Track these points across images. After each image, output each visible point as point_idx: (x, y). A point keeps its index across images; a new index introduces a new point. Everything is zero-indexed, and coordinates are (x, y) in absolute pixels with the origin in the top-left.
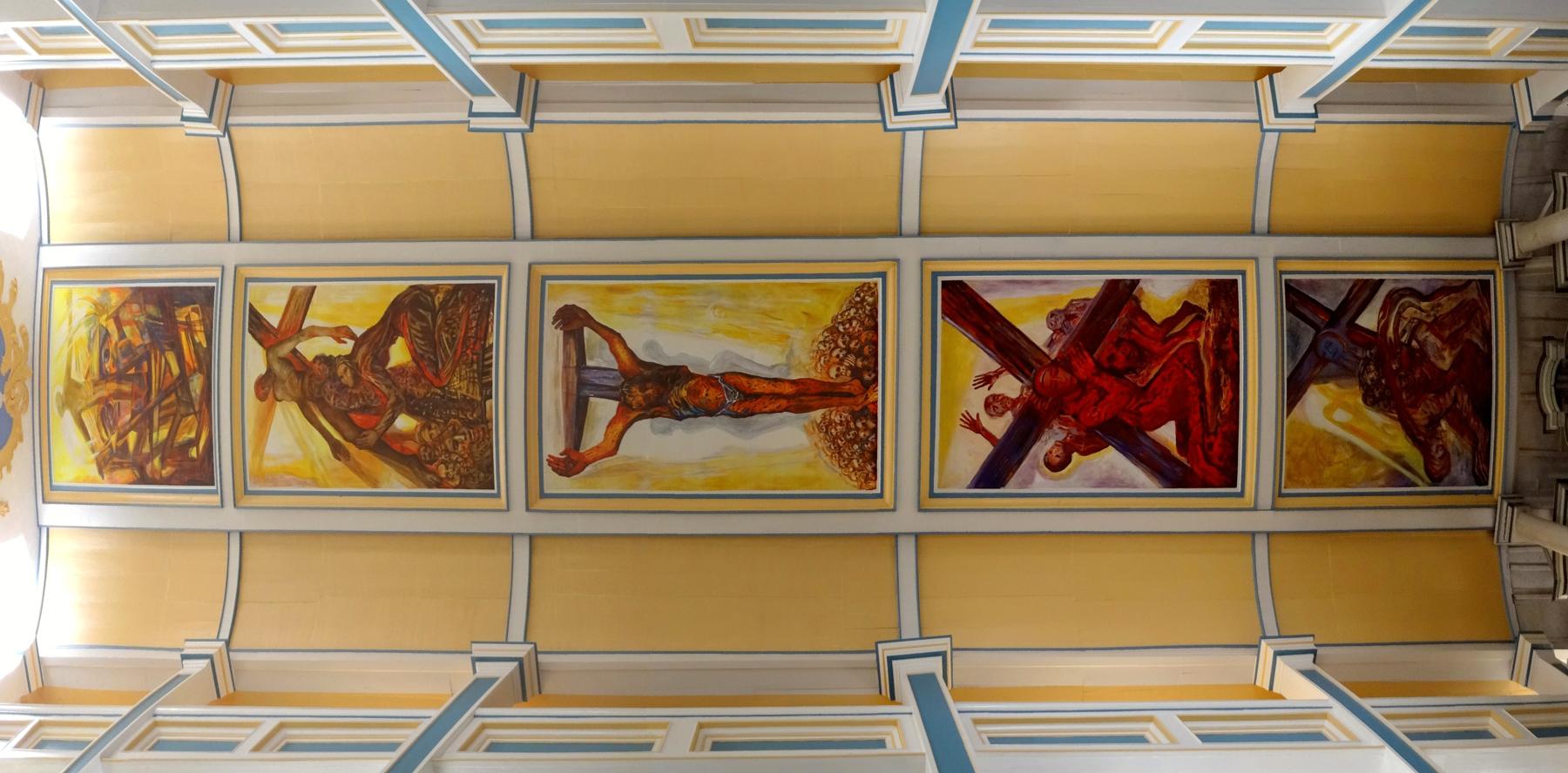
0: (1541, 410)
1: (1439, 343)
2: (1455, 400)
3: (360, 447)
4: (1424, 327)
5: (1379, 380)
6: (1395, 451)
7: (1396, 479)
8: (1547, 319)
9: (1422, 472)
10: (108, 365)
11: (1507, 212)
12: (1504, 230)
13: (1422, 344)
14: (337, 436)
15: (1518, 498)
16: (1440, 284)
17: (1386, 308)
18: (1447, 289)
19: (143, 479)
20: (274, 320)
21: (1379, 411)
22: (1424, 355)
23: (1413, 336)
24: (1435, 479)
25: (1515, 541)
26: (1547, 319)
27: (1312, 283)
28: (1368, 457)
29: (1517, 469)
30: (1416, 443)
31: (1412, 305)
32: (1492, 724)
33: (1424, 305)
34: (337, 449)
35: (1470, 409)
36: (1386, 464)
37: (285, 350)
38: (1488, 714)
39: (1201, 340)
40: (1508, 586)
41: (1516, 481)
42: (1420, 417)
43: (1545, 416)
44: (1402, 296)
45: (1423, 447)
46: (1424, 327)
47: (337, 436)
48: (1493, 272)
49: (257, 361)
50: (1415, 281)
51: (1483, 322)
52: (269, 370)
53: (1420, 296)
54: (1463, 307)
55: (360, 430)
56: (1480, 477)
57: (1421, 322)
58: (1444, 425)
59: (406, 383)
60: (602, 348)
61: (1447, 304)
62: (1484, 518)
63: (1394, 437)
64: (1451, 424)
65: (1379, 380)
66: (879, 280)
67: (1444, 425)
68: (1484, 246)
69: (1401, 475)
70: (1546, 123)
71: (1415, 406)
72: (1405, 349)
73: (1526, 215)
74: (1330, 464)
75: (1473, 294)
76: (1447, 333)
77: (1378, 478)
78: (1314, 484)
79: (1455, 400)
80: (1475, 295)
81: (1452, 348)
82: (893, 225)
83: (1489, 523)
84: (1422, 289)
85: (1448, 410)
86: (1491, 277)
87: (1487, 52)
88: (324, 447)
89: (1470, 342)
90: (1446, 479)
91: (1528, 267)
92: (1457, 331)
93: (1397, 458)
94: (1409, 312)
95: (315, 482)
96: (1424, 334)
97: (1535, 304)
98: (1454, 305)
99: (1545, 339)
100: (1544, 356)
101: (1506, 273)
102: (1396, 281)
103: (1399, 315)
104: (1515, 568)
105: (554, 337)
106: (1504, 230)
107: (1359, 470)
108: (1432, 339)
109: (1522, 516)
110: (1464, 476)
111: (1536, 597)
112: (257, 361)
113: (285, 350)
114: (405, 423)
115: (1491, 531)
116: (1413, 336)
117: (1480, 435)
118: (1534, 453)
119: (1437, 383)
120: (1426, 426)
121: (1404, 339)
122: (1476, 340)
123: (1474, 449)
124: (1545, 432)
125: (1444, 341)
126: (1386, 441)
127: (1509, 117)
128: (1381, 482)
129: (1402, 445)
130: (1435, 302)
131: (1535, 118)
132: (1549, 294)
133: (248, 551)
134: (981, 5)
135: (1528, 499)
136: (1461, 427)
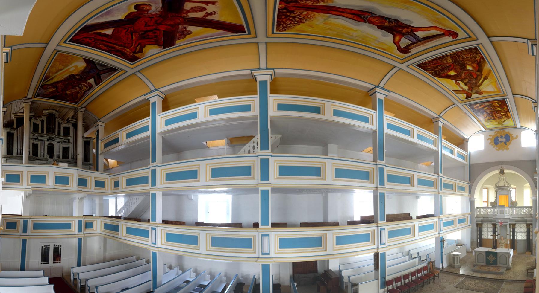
3: (482, 75)
7: (47, 78)
13: (76, 89)
14: (482, 79)
19: (508, 111)
20: (465, 95)
22: (73, 88)
23: (79, 87)
27: (112, 74)
28: (56, 72)
30: (54, 83)
34: (485, 78)
37: (470, 91)
39: (128, 50)
47: (482, 79)
49: (475, 96)
52: (476, 93)
55: (478, 76)
56: (39, 95)
57: (81, 89)
58: (54, 89)
59: (459, 70)
60: (402, 43)
62: (30, 96)
66: (275, 32)
67: (54, 89)
74: (60, 64)
77: (49, 73)
78: (56, 60)
82: (258, 67)
88: (486, 81)
93: (52, 79)
95: (496, 82)
105: (413, 51)
107: (54, 70)
110: (40, 92)
112: (475, 96)
113: (470, 91)
114: (469, 68)
115: (26, 97)
116: (79, 87)
129: (55, 80)
133: (517, 93)
134: (280, 1)
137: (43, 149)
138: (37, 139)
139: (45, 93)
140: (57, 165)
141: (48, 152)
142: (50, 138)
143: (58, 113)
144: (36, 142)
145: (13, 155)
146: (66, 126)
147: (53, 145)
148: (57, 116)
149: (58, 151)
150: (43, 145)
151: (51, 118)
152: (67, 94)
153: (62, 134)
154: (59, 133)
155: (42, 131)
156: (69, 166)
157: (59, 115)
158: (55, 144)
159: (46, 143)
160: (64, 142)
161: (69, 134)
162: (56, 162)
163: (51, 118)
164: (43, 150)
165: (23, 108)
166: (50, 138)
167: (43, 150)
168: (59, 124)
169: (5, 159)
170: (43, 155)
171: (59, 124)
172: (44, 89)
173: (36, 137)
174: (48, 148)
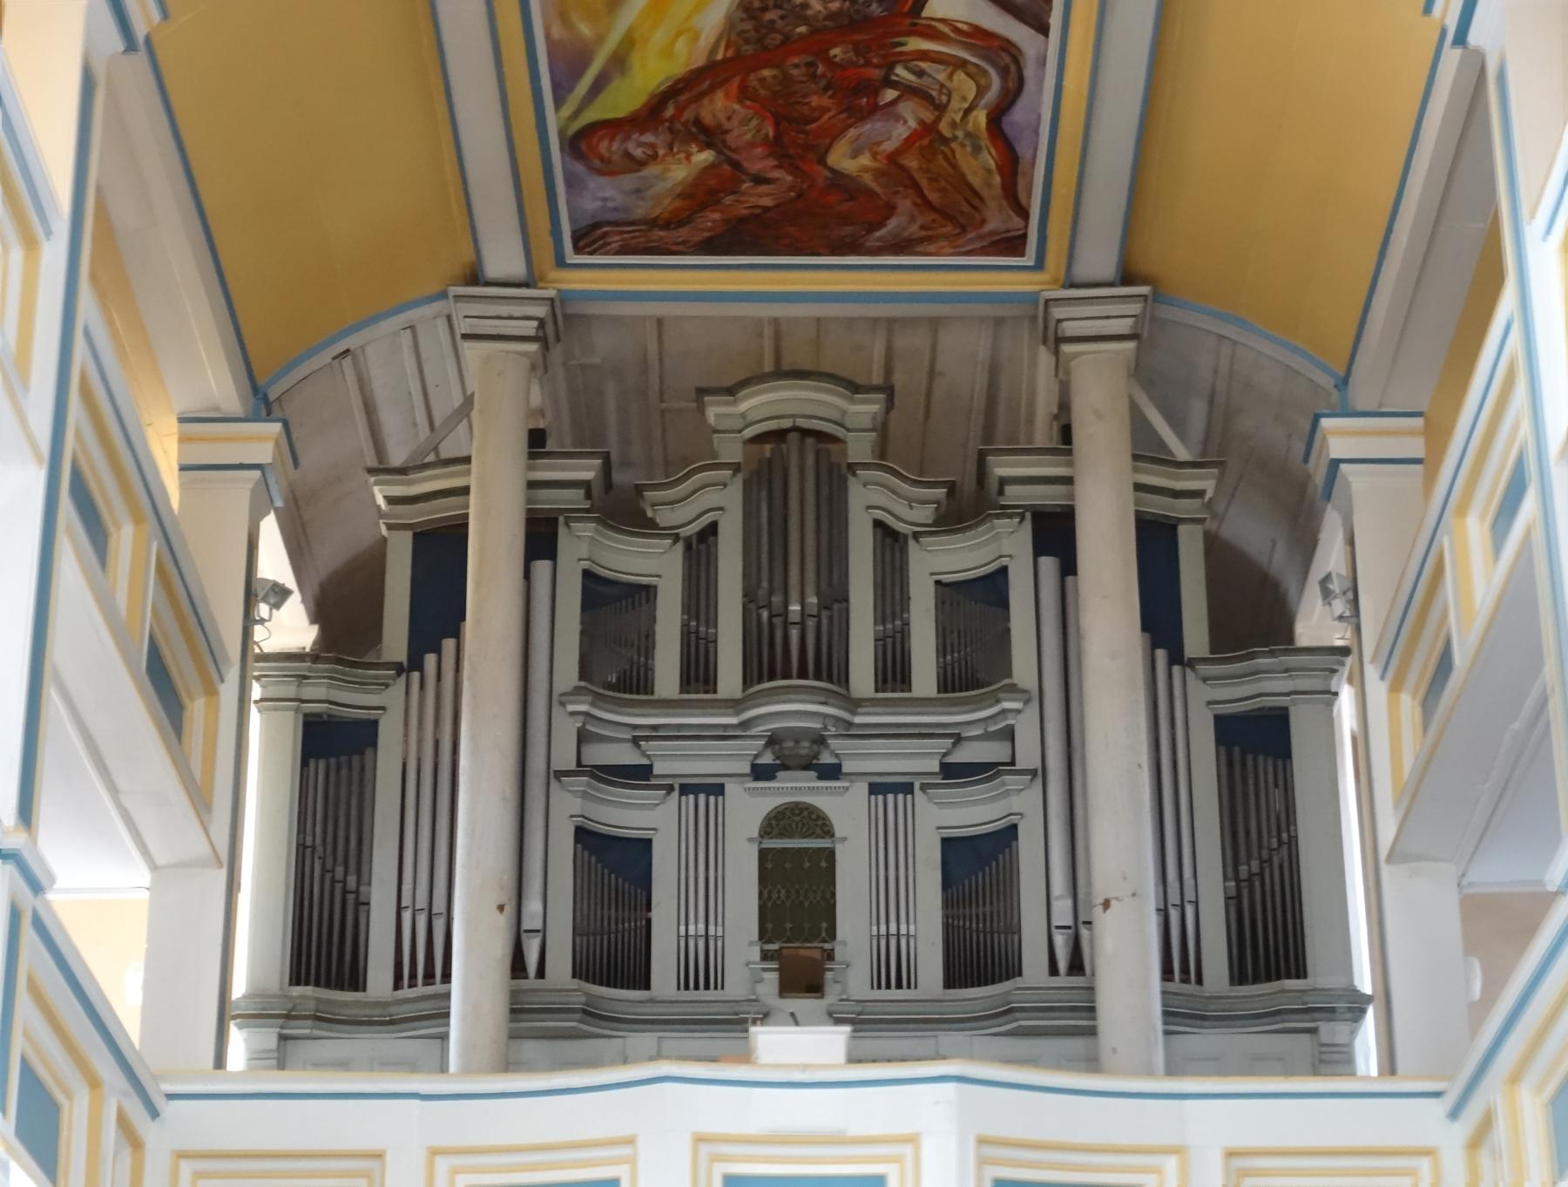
0: (746, 383)
1: (889, 146)
2: (759, 180)
4: (928, 116)
5: (805, 20)
6: (636, 59)
7: (569, 63)
8: (932, 373)
9: (592, 115)
10: (789, 744)
11: (1166, 312)
12: (1119, 314)
15: (559, 329)
16: (1023, 151)
17: (978, 36)
18: (1011, 165)
21: (730, 23)
23: (908, 91)
24: (580, 143)
25: (471, 350)
26: (932, 373)
29: (618, 320)
31: (981, 92)
32: (125, 538)
33: (980, 117)
35: (743, 211)
36: (600, 39)
38: (138, 519)
40: (366, 334)
41: (587, 319)
42: (718, 106)
43: (731, 391)
44: (1004, 72)
45: (650, 114)
46: (928, 116)
48: (1040, 265)
50: (1038, 100)
51: (930, 239)
53: (997, 117)
54: (972, 197)
56: (589, 237)
57: (941, 109)
58: (704, 157)
61: (980, 166)
62: (504, 259)
63: (667, 53)
64: (709, 169)
65: (805, 20)
67: (704, 157)
68: (1099, 259)
69: (577, 72)
70: (1319, 478)
71: (744, 94)
72: (877, 74)
73: (1150, 373)
75: (997, 219)
76: (912, 163)
77: (564, 17)
79: (759, 180)
80: (992, 225)
81: (878, 174)
83: (492, 270)
84: (1018, 115)
85: (736, 165)
86: (1028, 260)
87: (1462, 511)
89: (891, 209)
90: (579, 168)
91: (1042, 349)
92: (916, 186)
93: (619, 62)
94: (964, 86)
96: (911, 115)
97: (963, 355)
98: (976, 181)
99: (888, 390)
100: (854, 388)
101: (1032, 298)
102: (1042, 62)
103: (962, 64)
104: (406, 337)
106: (1119, 314)
108: (900, 132)
109: (526, 362)
110: (590, 205)
111: (356, 402)
115: (474, 276)
116: (908, 91)
117: (683, 233)
118: (653, 347)
119: (796, 140)
120: (698, 122)
121: (901, 72)
122: (893, 224)
123: (653, 223)
124: (702, 392)
125: (893, 158)
126: (659, 37)
127: (1362, 393)
128: (558, 32)
130: (985, 141)
131: (1335, 464)
132: (981, 381)
135: (557, 353)
136: (700, 195)
137: (706, 892)
138: (638, 775)
139: (641, 210)
140: (746, 1057)
141: (771, 923)
142: (790, 754)
143: (866, 409)
144: (626, 814)
145: (355, 979)
146: (960, 556)
147: (817, 823)
148: (859, 448)
149: (890, 895)
150: (706, 843)
151: (794, 477)
152: (841, 183)
153: (924, 677)
154: (894, 670)
155: (698, 672)
156: (854, 1059)
157: (882, 430)
158: (847, 810)
159: (747, 809)
160: (953, 772)
161: (1003, 665)
162: (714, 1023)
163: (794, 477)
164: (708, 898)
165: (475, 422)
166: (790, 754)
167: (480, 879)
168: (891, 543)
169: (268, 1037)
170: (701, 972)
171: (891, 543)
172: (607, 169)
173: (626, 756)
174: (771, 867)
